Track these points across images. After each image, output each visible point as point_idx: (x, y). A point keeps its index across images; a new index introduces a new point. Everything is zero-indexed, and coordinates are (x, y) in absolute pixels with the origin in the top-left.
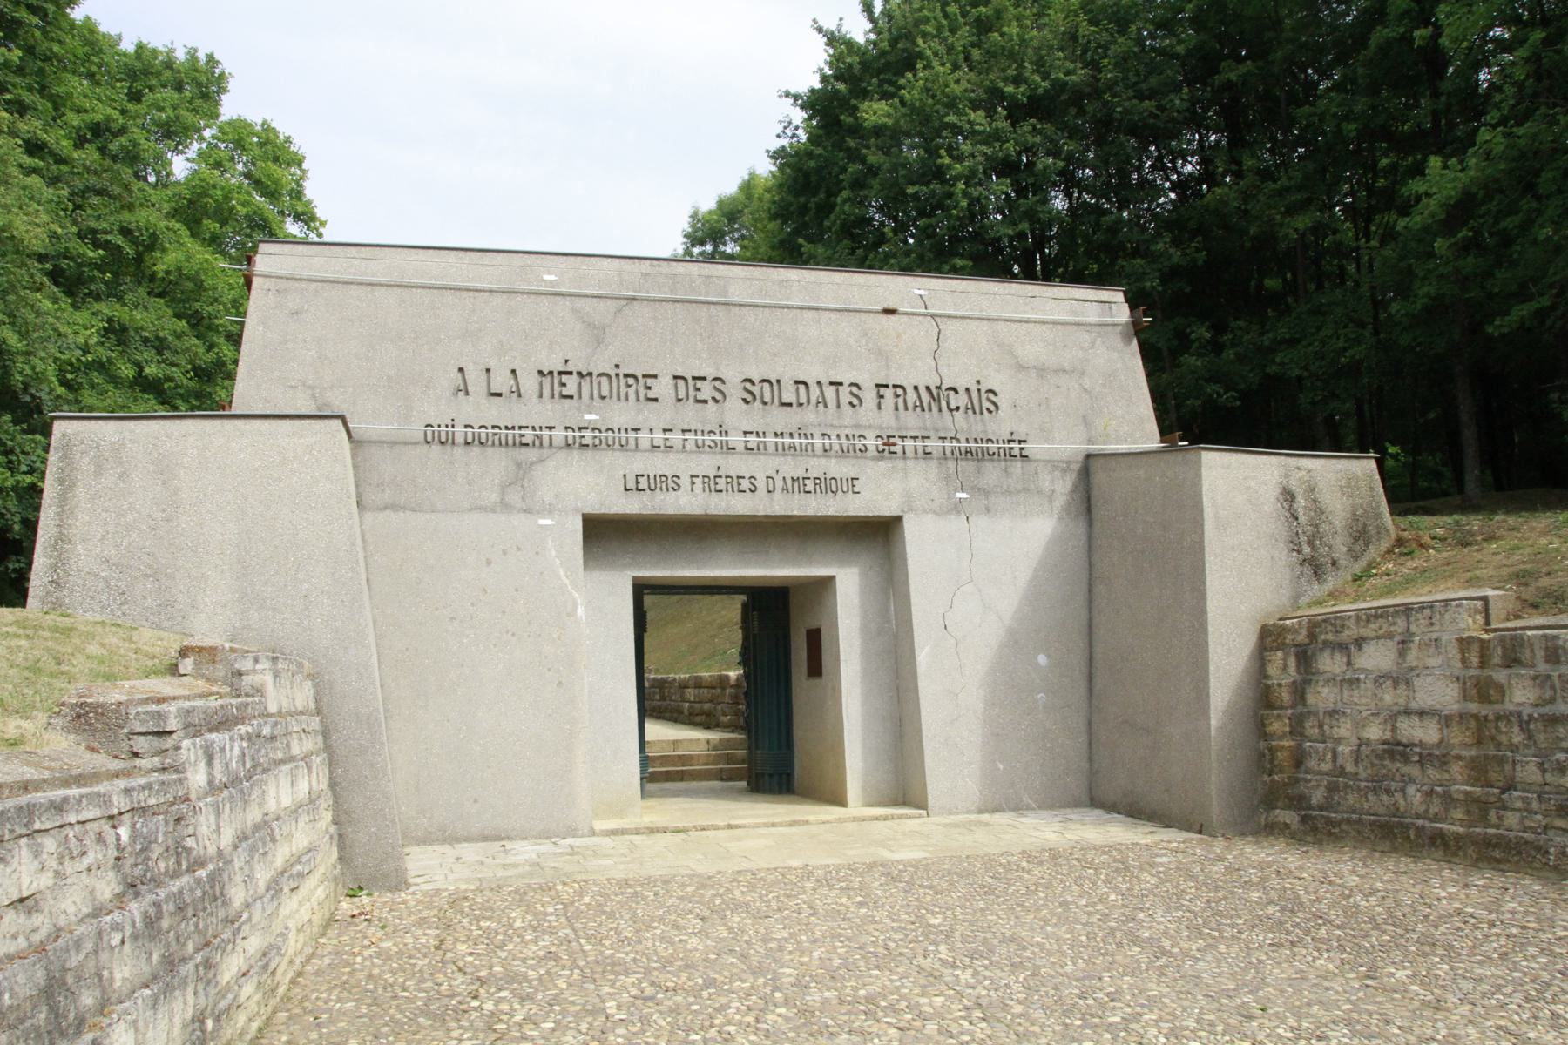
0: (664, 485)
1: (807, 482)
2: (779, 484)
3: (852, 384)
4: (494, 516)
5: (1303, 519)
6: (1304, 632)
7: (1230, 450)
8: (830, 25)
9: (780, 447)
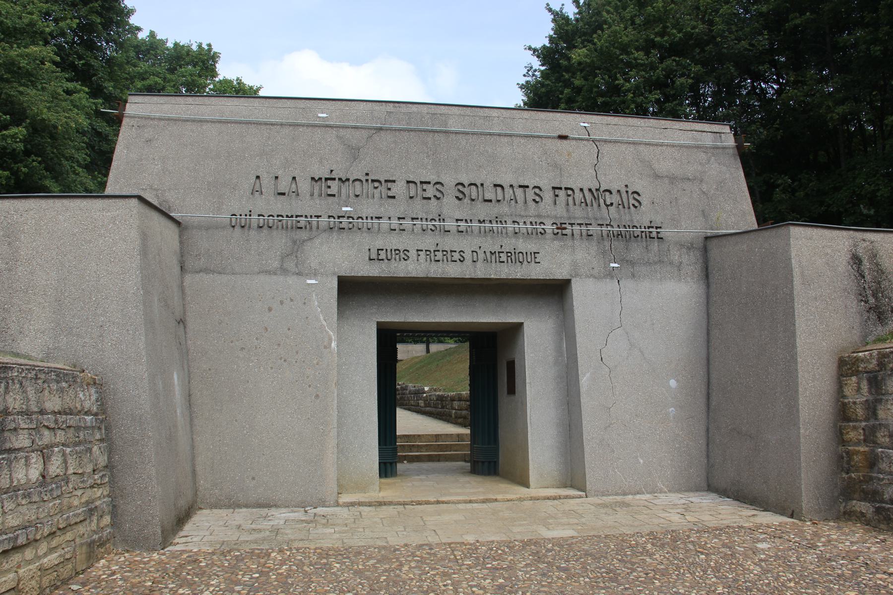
0: (397, 257)
1: (501, 255)
2: (481, 256)
3: (535, 187)
4: (275, 277)
5: (868, 278)
6: (874, 362)
7: (812, 226)
8: (556, 8)
9: (483, 229)
